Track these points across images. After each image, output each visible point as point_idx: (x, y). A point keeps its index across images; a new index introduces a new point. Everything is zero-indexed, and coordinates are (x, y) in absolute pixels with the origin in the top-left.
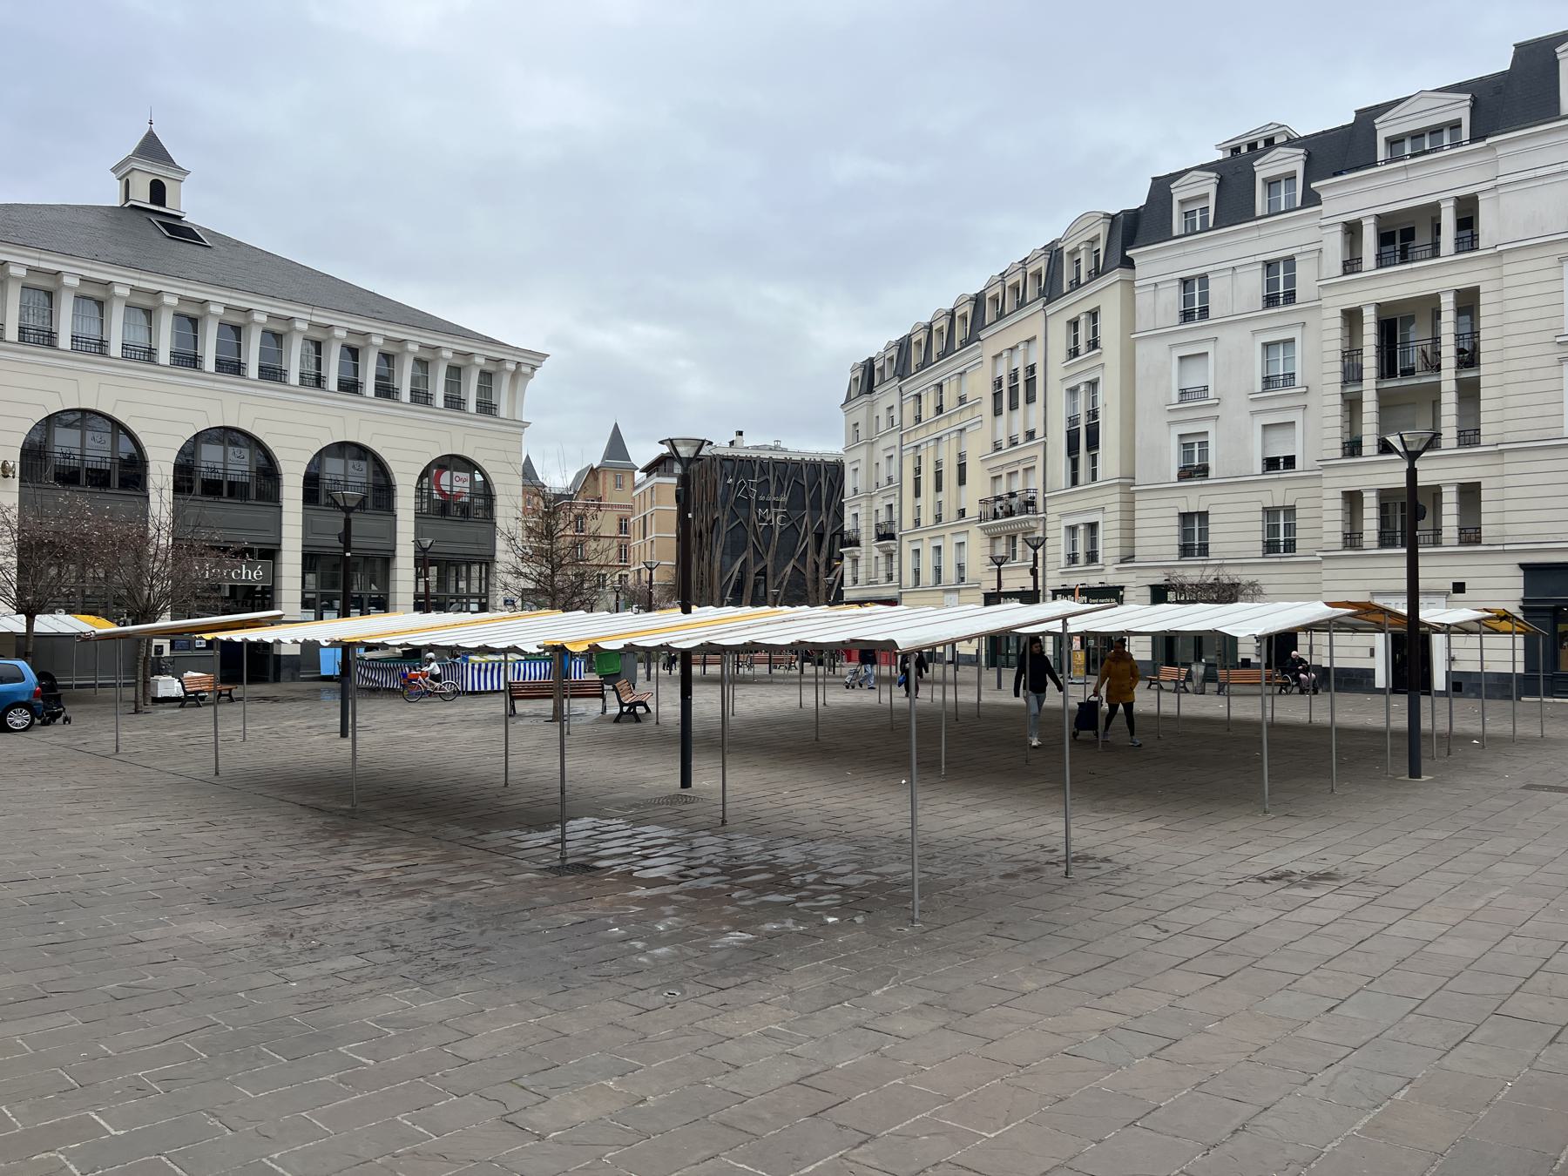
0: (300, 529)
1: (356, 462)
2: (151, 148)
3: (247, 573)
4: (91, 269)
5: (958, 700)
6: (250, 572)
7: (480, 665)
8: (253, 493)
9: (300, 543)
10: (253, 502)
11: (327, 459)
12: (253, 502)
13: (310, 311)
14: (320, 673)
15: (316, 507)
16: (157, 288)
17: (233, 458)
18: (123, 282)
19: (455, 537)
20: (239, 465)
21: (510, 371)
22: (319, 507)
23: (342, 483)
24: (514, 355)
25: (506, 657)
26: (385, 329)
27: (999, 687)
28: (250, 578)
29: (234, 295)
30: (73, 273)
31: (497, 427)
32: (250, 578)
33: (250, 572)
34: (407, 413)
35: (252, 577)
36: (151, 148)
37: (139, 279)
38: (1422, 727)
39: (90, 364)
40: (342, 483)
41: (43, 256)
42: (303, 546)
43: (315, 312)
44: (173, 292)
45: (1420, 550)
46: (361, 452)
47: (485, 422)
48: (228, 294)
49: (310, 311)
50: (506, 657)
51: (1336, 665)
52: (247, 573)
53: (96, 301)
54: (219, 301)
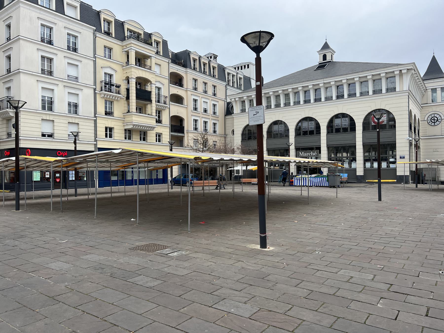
0: (326, 141)
1: (311, 122)
2: (326, 46)
3: (313, 154)
4: (274, 89)
5: (269, 198)
6: (313, 154)
7: (299, 178)
8: (349, 130)
9: (362, 142)
10: (302, 136)
11: (336, 119)
12: (302, 136)
13: (323, 80)
14: (112, 176)
15: (333, 134)
16: (353, 77)
17: (344, 121)
18: (321, 83)
19: (308, 141)
20: (345, 122)
21: (357, 81)
22: (333, 134)
23: (307, 128)
24: (398, 68)
25: (308, 176)
26: (358, 75)
27: (380, 199)
28: (313, 155)
29: (347, 76)
30: (310, 84)
31: (356, 100)
32: (313, 155)
33: (313, 154)
34: (284, 110)
35: (314, 155)
36: (326, 46)
37: (265, 91)
38: (260, 246)
39: (377, 96)
40: (278, 131)
41: (385, 69)
42: (327, 145)
43: (324, 80)
44: (332, 81)
45: (15, 138)
46: (344, 115)
47: (391, 95)
48: (346, 76)
49: (323, 80)
50: (308, 176)
51: (145, 186)
52: (313, 154)
53: (364, 82)
54: (344, 79)
